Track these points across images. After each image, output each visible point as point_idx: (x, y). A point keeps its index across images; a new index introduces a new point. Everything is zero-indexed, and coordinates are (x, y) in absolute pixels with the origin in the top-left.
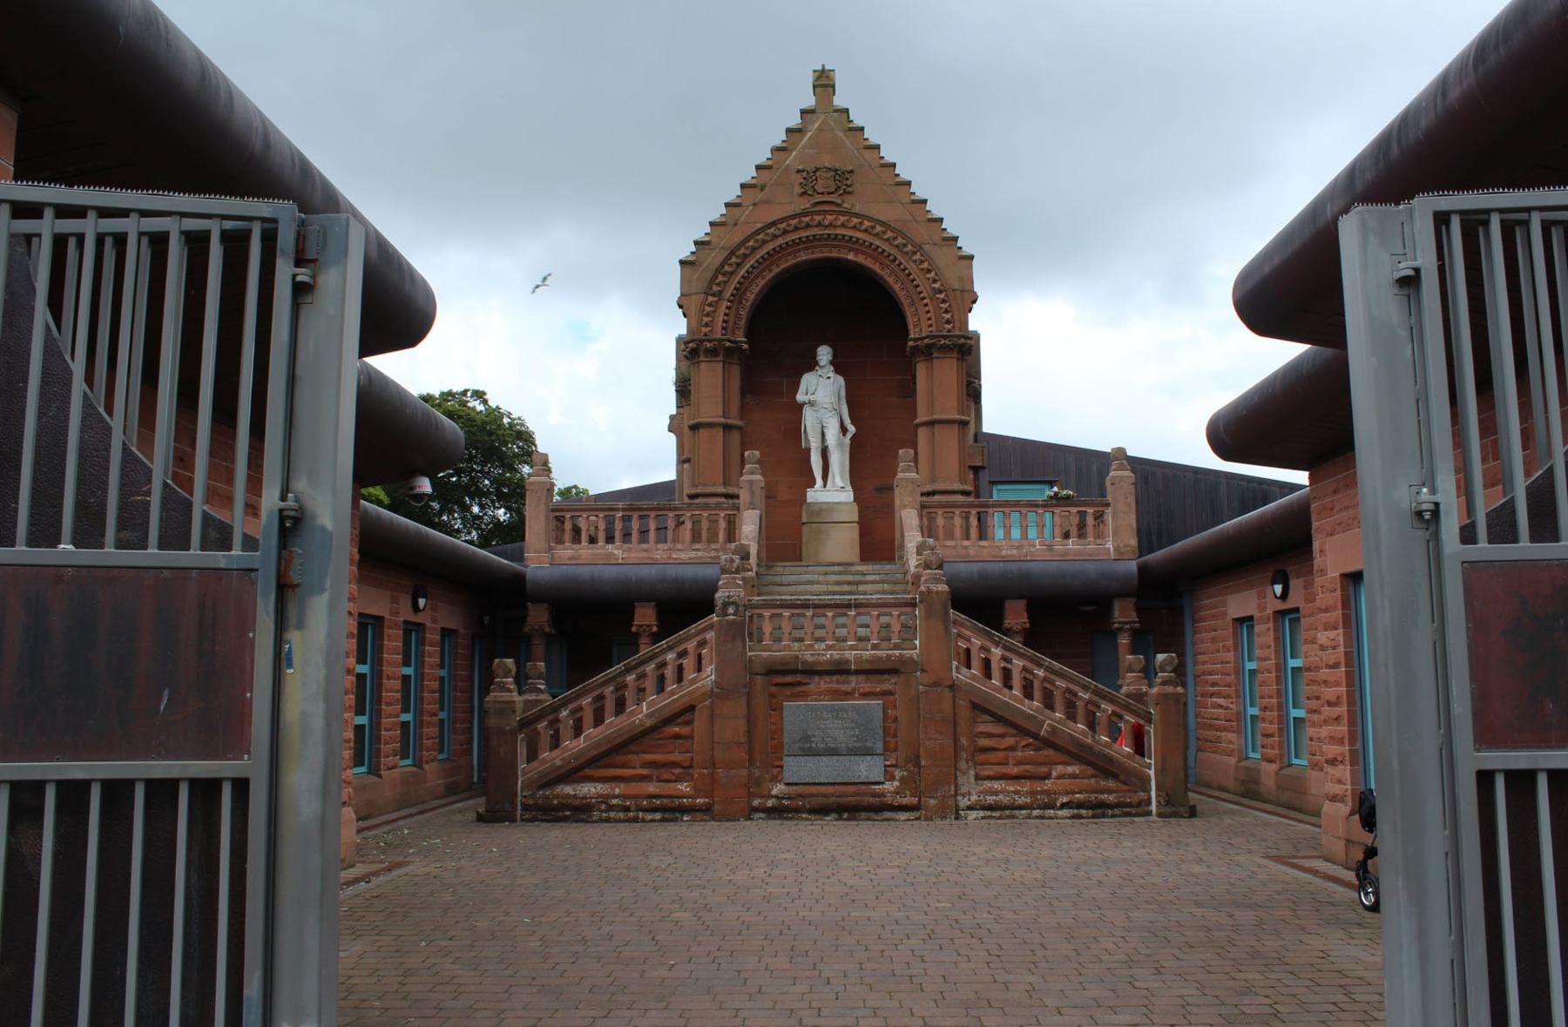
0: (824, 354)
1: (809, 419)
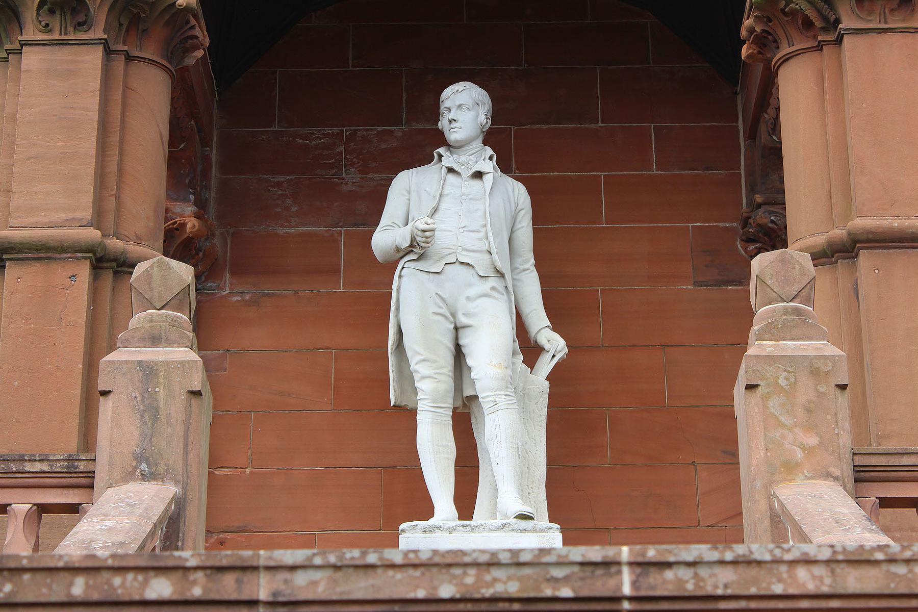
0: (465, 107)
1: (414, 301)
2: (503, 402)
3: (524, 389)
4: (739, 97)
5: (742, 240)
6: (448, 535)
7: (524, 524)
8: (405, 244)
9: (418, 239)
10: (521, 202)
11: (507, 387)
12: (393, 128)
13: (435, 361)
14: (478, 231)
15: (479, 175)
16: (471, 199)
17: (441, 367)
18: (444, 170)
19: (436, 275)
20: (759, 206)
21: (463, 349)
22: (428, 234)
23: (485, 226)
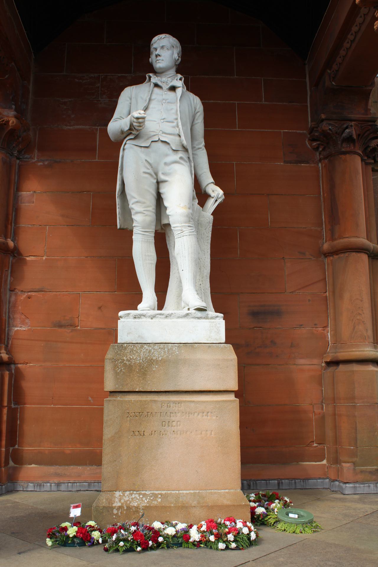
0: (165, 49)
1: (132, 163)
2: (187, 231)
3: (198, 220)
4: (307, 66)
5: (309, 140)
6: (150, 320)
7: (199, 314)
8: (126, 128)
9: (135, 124)
10: (198, 108)
11: (190, 221)
12: (126, 75)
13: (144, 203)
14: (173, 122)
15: (173, 89)
16: (168, 103)
17: (148, 207)
18: (152, 85)
19: (146, 149)
20: (323, 120)
21: (162, 196)
22: (140, 120)
23: (177, 119)
